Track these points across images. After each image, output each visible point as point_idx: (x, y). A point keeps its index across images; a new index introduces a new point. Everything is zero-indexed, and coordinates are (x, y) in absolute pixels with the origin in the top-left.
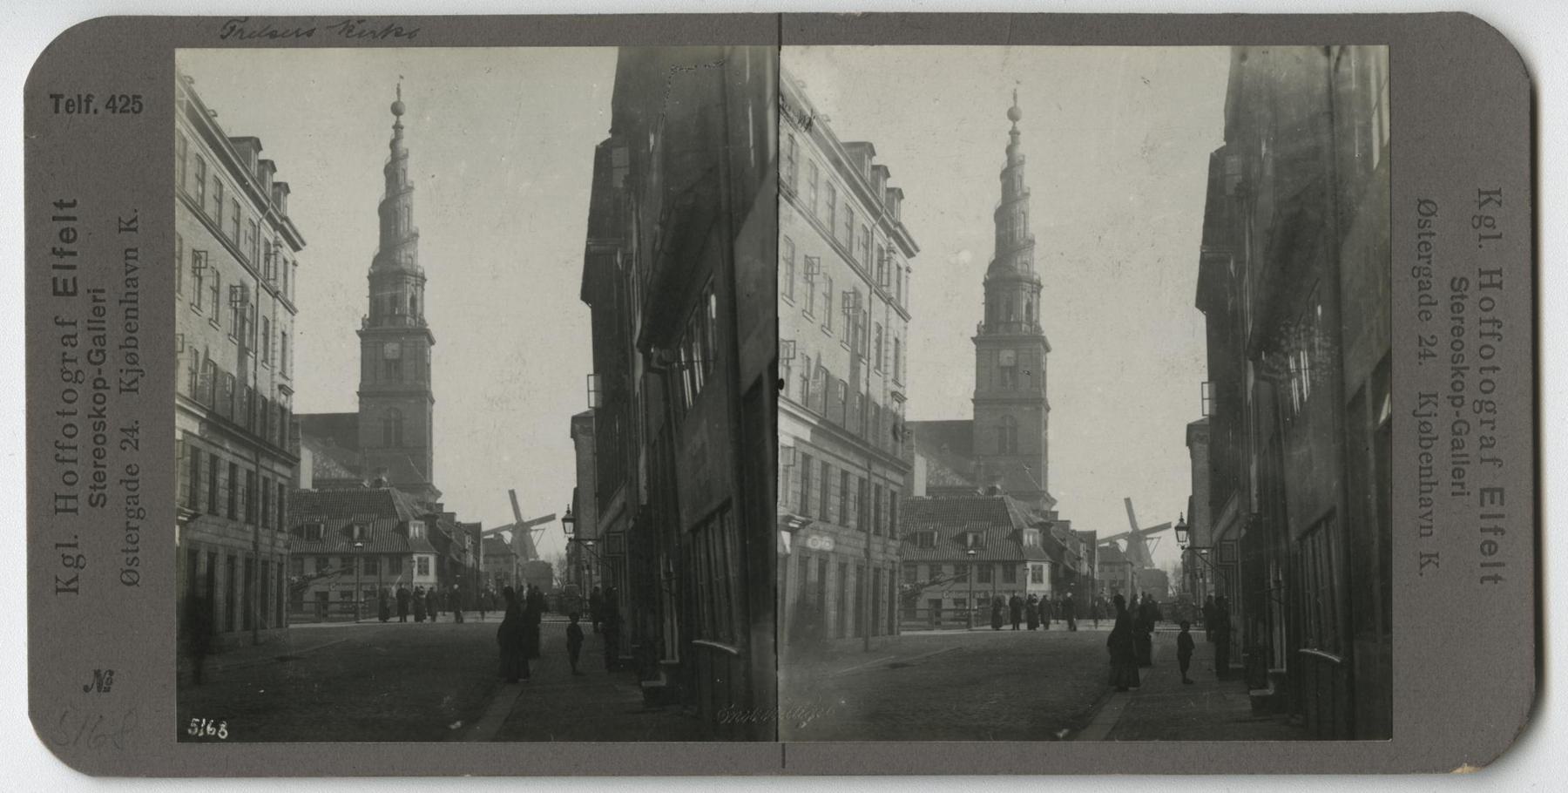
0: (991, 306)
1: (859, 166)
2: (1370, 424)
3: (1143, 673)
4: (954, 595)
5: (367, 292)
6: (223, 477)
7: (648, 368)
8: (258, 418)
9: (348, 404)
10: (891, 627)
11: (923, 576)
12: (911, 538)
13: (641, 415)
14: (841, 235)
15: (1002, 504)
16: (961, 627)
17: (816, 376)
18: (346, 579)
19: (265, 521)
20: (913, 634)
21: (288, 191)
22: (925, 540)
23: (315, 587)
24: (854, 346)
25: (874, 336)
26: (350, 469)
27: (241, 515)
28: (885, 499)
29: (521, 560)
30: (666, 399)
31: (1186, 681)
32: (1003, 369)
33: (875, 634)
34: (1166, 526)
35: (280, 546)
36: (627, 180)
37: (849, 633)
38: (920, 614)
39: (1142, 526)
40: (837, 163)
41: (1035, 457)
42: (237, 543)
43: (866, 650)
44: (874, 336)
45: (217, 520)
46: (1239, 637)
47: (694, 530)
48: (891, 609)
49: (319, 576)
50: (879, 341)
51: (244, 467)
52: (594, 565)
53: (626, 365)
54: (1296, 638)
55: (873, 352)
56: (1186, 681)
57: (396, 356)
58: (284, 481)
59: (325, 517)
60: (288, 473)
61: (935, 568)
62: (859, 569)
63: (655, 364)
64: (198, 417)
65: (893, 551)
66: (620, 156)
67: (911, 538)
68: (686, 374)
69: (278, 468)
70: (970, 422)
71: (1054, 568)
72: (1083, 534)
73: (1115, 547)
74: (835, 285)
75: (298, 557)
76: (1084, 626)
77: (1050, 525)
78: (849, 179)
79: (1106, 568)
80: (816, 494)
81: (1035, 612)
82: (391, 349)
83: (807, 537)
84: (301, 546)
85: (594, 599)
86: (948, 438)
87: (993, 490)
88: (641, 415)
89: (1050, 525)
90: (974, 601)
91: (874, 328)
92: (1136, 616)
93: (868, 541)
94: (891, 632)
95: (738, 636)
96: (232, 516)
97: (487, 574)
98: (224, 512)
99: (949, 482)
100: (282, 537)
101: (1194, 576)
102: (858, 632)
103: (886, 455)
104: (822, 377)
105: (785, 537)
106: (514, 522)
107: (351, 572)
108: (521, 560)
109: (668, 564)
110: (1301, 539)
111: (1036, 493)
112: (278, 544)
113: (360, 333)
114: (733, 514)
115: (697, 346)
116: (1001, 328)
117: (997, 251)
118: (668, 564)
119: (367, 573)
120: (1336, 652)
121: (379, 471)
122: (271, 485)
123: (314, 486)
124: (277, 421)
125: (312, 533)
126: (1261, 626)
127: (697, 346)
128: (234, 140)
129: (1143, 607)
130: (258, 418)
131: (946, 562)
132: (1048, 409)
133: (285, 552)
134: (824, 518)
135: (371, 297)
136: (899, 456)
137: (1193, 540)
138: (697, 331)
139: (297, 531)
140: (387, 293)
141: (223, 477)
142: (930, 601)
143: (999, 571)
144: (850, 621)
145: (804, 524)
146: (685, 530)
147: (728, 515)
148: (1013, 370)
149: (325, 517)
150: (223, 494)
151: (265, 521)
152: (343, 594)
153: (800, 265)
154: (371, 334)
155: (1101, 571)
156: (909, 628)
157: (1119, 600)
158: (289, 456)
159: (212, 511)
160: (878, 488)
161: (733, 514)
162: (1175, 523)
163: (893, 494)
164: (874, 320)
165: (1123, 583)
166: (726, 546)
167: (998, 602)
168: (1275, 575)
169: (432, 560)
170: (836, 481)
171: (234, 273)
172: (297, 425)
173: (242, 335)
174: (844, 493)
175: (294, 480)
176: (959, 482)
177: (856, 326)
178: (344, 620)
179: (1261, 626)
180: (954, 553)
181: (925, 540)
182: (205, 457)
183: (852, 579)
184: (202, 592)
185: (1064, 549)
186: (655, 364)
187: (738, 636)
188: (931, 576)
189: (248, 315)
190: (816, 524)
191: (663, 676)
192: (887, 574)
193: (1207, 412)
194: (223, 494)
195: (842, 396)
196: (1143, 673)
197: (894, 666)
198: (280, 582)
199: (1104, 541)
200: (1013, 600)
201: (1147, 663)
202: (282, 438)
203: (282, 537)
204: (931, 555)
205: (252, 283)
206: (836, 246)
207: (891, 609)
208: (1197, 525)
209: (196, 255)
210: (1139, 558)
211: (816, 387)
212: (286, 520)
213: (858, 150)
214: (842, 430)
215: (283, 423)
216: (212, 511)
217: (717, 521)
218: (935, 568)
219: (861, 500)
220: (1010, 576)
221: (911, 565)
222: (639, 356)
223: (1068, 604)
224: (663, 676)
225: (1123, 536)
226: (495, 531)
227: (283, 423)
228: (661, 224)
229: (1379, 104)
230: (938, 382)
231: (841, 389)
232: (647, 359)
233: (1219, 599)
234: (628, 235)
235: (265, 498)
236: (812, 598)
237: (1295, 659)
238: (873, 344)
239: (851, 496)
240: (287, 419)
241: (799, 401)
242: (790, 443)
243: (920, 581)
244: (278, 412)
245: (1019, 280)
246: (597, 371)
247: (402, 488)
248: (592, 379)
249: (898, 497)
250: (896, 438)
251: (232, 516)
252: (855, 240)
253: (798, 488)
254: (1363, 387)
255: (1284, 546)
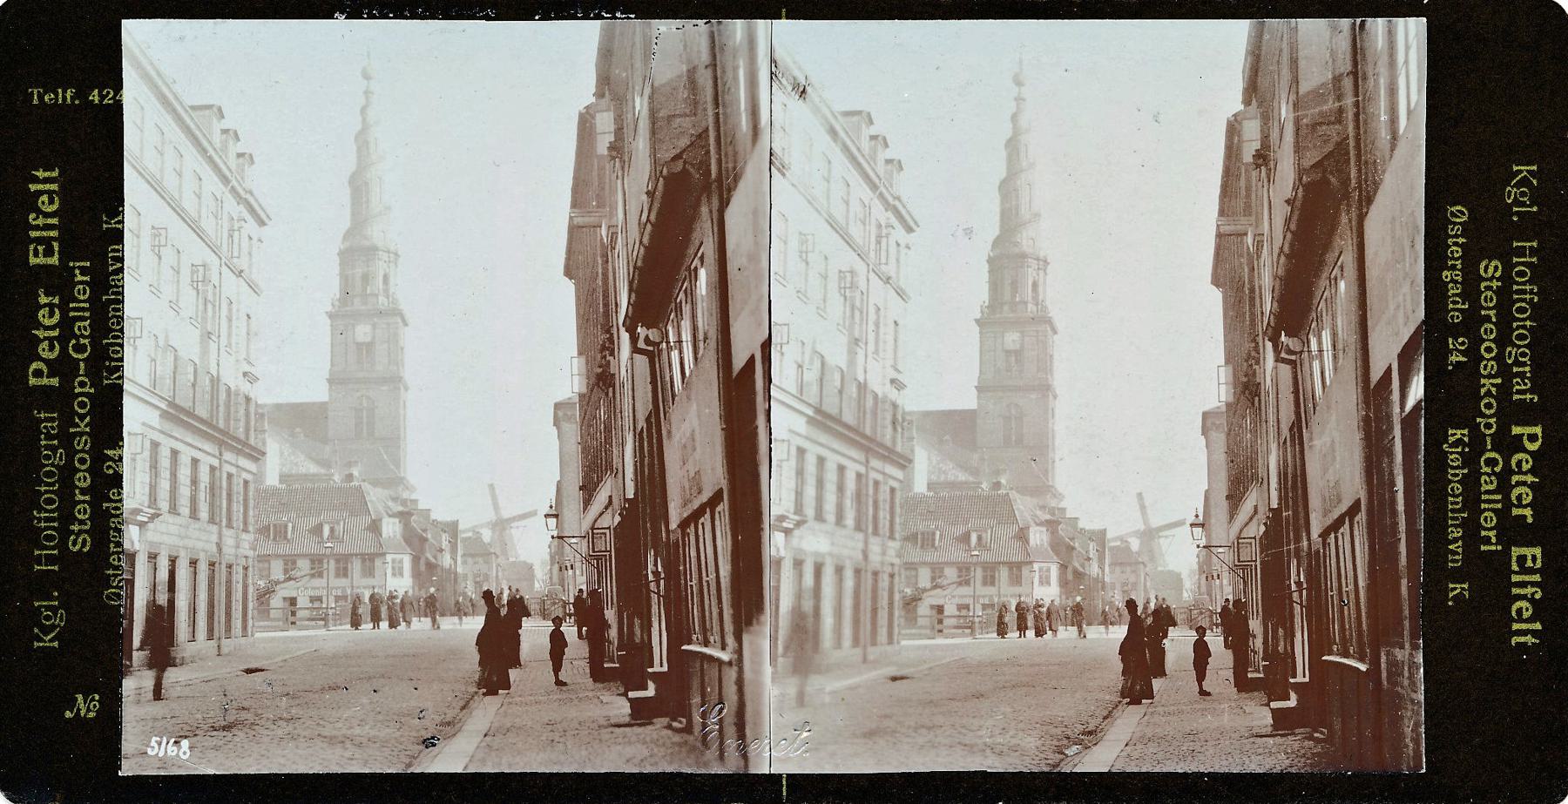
0: (995, 286)
1: (854, 137)
2: (1397, 410)
3: (1157, 684)
4: (957, 601)
5: (337, 270)
6: (184, 473)
7: (635, 350)
8: (222, 409)
9: (316, 391)
10: (245, 628)
11: (277, 571)
12: (911, 538)
13: (627, 401)
14: (838, 213)
15: (1006, 500)
16: (963, 635)
17: (812, 360)
18: (317, 582)
19: (229, 519)
20: (914, 646)
21: (252, 162)
22: (927, 541)
23: (930, 600)
24: (851, 329)
25: (872, 317)
26: (319, 463)
27: (204, 514)
28: (884, 495)
29: (501, 560)
30: (654, 382)
31: (1203, 693)
32: (1008, 352)
33: (874, 644)
34: (1180, 523)
35: (246, 549)
36: (612, 147)
37: (847, 641)
38: (273, 614)
39: (506, 514)
40: (833, 132)
41: (1038, 451)
42: (200, 545)
43: (865, 660)
44: (872, 317)
45: (178, 520)
46: (613, 633)
47: (684, 525)
48: (891, 615)
49: (936, 587)
50: (877, 324)
51: (207, 461)
52: (578, 565)
53: (609, 347)
54: (1319, 645)
55: (871, 337)
56: (1203, 693)
57: (368, 339)
58: (249, 477)
59: (293, 515)
60: (899, 474)
61: (937, 570)
62: (858, 572)
63: (641, 344)
64: (157, 407)
65: (892, 552)
66: (605, 123)
67: (264, 531)
68: (675, 355)
69: (244, 462)
70: (973, 412)
71: (416, 560)
72: (447, 524)
73: (478, 538)
74: (183, 257)
75: (264, 559)
76: (448, 623)
77: (409, 514)
78: (846, 149)
79: (1118, 569)
80: (810, 491)
81: (386, 610)
82: (363, 332)
83: (801, 538)
84: (268, 548)
85: (579, 599)
86: (954, 428)
87: (997, 485)
88: (627, 401)
89: (409, 514)
90: (978, 607)
91: (872, 310)
92: (1149, 620)
93: (866, 543)
94: (890, 641)
95: (730, 640)
96: (194, 514)
97: (465, 576)
98: (185, 511)
99: (951, 478)
100: (894, 546)
101: (1210, 578)
102: (856, 641)
103: (238, 440)
104: (817, 364)
105: (778, 538)
106: (1143, 527)
107: (320, 575)
108: (501, 560)
109: (656, 565)
110: (1324, 535)
111: (1041, 488)
112: (240, 545)
113: (331, 316)
114: (723, 507)
115: (686, 325)
116: (1006, 308)
117: (1002, 226)
118: (656, 565)
119: (985, 583)
120: (1362, 660)
121: (349, 464)
122: (235, 480)
123: (281, 482)
124: (242, 412)
125: (280, 533)
126: (637, 622)
127: (686, 325)
128: (193, 108)
129: (1156, 612)
130: (222, 409)
131: (278, 556)
132: (1055, 397)
133: (250, 553)
134: (819, 517)
135: (341, 275)
136: (899, 449)
137: (1208, 537)
138: (686, 309)
139: (264, 531)
140: (359, 271)
141: (184, 473)
142: (932, 607)
143: (1004, 574)
144: (847, 631)
145: (799, 524)
146: (673, 526)
147: (719, 509)
148: (1018, 354)
149: (293, 515)
150: (185, 491)
151: (229, 519)
152: (960, 607)
153: (794, 243)
154: (343, 316)
155: (464, 563)
156: (912, 637)
157: (1131, 605)
158: (901, 456)
159: (173, 510)
160: (876, 483)
161: (723, 507)
162: (1192, 519)
163: (893, 490)
164: (871, 302)
165: (1135, 584)
166: (715, 547)
167: (1004, 608)
168: (1296, 574)
169: (1054, 571)
170: (831, 477)
171: (196, 252)
172: (262, 415)
173: (205, 319)
174: (841, 488)
175: (907, 483)
176: (962, 477)
177: (853, 308)
178: (313, 628)
179: (637, 622)
180: (958, 555)
181: (927, 541)
182: (165, 453)
183: (849, 583)
184: (162, 599)
185: (426, 540)
186: (641, 344)
187: (730, 640)
188: (933, 579)
189: (858, 304)
190: (811, 523)
191: (1293, 696)
192: (886, 577)
193: (1223, 398)
194: (185, 491)
195: (838, 383)
196: (1157, 684)
197: (894, 679)
198: (245, 587)
199: (1115, 539)
200: (372, 597)
201: (516, 662)
202: (247, 430)
203: (894, 546)
204: (284, 549)
205: (861, 267)
206: (832, 223)
207: (891, 615)
208: (1213, 521)
209: (157, 231)
210: (1152, 559)
211: (165, 369)
212: (251, 520)
213: (855, 119)
214: (839, 421)
215: (247, 415)
216: (173, 510)
217: (708, 516)
218: (937, 570)
219: (859, 497)
220: (1016, 580)
221: (911, 567)
222: (625, 336)
223: (1077, 609)
224: (1293, 696)
225: (1137, 533)
226: (1121, 539)
227: (247, 415)
228: (648, 193)
229: (1406, 62)
230: (938, 371)
231: (837, 377)
232: (634, 339)
233: (1237, 602)
234: (613, 208)
235: (229, 495)
236: (808, 605)
237: (1316, 664)
238: (871, 327)
239: (202, 486)
240: (252, 410)
241: (794, 391)
242: (138, 429)
243: (921, 585)
244: (242, 400)
245: (1024, 256)
246: (1227, 362)
247: (376, 483)
248: (575, 361)
249: (898, 494)
250: (895, 429)
251: (194, 514)
252: (852, 215)
253: (792, 484)
254: (1389, 369)
255: (1305, 543)
